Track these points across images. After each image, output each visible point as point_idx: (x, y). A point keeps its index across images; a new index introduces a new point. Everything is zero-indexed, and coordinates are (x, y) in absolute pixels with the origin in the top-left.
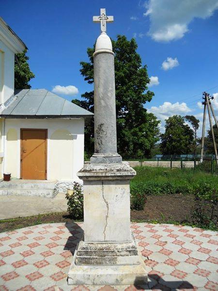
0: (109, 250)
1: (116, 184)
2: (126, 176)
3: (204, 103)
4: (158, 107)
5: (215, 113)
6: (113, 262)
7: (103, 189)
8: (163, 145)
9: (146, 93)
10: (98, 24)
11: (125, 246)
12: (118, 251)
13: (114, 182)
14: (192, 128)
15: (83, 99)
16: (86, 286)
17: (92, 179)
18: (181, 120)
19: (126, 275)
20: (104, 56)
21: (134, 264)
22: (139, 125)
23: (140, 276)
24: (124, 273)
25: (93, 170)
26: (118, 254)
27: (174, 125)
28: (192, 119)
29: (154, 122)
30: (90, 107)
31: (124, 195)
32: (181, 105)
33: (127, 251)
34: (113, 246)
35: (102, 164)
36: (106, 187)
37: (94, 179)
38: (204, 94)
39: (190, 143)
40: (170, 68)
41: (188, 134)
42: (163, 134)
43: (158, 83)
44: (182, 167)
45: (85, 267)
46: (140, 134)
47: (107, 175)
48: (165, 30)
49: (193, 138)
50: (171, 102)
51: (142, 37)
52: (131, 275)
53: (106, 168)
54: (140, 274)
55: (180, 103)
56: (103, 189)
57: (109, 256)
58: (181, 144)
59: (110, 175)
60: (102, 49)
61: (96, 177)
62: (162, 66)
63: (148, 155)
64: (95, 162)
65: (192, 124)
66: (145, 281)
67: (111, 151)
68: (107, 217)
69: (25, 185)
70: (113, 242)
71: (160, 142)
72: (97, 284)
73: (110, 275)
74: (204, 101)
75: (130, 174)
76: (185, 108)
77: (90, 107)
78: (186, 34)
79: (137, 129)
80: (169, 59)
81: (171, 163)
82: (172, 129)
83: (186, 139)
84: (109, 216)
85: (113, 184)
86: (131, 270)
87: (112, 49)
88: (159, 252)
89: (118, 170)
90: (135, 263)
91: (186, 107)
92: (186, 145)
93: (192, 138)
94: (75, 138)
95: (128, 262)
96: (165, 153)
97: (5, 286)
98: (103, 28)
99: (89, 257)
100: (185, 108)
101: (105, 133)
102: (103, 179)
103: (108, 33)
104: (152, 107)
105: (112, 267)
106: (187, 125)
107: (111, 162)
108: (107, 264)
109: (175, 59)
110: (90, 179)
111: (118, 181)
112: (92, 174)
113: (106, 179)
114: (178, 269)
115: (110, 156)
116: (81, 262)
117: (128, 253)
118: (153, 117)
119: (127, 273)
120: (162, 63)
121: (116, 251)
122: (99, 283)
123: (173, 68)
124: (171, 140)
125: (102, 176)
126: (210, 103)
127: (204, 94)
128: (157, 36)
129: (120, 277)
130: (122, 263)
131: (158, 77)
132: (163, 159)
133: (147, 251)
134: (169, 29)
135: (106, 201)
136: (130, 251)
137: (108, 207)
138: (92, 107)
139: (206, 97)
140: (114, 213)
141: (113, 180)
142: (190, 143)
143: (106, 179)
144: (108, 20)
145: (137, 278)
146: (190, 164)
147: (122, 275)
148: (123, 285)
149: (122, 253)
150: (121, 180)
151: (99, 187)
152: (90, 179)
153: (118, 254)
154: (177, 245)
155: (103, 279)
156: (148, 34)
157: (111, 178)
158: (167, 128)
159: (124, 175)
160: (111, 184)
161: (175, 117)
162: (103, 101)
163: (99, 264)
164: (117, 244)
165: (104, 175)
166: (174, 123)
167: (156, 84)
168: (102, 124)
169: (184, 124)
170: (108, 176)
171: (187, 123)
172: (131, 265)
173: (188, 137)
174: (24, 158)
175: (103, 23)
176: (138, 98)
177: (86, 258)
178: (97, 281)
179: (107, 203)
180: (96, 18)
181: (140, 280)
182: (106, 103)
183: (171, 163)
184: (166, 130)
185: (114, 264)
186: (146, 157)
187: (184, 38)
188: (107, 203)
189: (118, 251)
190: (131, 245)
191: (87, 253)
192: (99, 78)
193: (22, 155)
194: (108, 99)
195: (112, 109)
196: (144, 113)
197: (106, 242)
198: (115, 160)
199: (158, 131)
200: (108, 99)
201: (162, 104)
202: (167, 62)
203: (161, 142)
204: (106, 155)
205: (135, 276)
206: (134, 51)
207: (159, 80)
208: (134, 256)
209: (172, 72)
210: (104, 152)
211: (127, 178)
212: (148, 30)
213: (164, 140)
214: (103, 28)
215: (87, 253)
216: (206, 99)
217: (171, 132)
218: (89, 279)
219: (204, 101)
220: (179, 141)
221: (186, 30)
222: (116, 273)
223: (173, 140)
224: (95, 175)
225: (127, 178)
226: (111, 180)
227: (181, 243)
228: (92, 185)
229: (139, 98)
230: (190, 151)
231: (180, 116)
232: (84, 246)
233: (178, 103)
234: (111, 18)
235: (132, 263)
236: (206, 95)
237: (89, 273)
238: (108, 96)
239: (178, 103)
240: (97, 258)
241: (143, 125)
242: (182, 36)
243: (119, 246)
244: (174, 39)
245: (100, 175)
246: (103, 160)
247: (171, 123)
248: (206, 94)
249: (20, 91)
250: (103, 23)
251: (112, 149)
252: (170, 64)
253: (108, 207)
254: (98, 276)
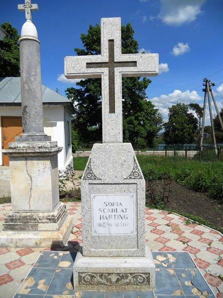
0: (31, 218)
1: (38, 160)
2: (45, 152)
3: (205, 90)
4: (167, 94)
5: (215, 99)
6: (35, 228)
7: (26, 165)
8: (166, 134)
9: (142, 80)
10: (23, 12)
11: (46, 214)
12: (40, 219)
13: (37, 158)
14: (196, 115)
15: (78, 87)
16: (8, 248)
17: (17, 155)
18: (184, 108)
19: (44, 239)
20: (26, 42)
21: (53, 231)
22: (136, 113)
23: (56, 240)
24: (42, 237)
25: (18, 147)
26: (40, 221)
27: (178, 114)
28: (195, 106)
29: (151, 111)
30: (85, 95)
31: (45, 170)
32: (191, 93)
33: (47, 219)
34: (36, 214)
35: (25, 142)
36: (29, 162)
37: (17, 155)
38: (204, 81)
39: (193, 132)
40: (180, 54)
41: (192, 122)
42: (166, 124)
43: (168, 70)
44: (175, 155)
45: (10, 232)
46: (136, 122)
47: (28, 151)
48: (177, 13)
49: (197, 127)
50: (181, 90)
51: (152, 20)
52: (49, 239)
53: (29, 145)
54: (56, 239)
55: (191, 91)
56: (26, 165)
57: (32, 223)
58: (184, 133)
59: (30, 151)
60: (25, 36)
61: (18, 153)
62: (172, 51)
63: (151, 145)
64: (19, 140)
65: (196, 112)
66: (61, 245)
67: (35, 131)
68: (31, 189)
69: (4, 171)
70: (38, 211)
71: (163, 131)
72: (19, 247)
73: (30, 239)
74: (204, 87)
75: (47, 151)
76: (195, 96)
77: (85, 95)
78: (198, 16)
79: (133, 118)
80: (180, 45)
81: (166, 152)
82: (175, 118)
83: (189, 128)
84: (33, 188)
85: (36, 160)
86: (49, 235)
87: (37, 37)
88: (176, 240)
89: (39, 148)
90: (54, 229)
91: (197, 95)
92: (189, 134)
93: (196, 127)
94: (55, 125)
95: (48, 229)
96: (167, 143)
97: (9, 269)
98: (28, 16)
99: (13, 223)
100: (195, 96)
101: (29, 114)
102: (25, 155)
103: (34, 21)
104: (162, 96)
105: (33, 232)
106: (191, 114)
107: (34, 140)
108: (30, 230)
109: (187, 44)
110: (13, 155)
111: (39, 157)
112: (14, 151)
113: (27, 155)
114: (200, 258)
115: (33, 135)
116: (6, 228)
117: (48, 221)
118: (151, 105)
119: (45, 237)
120: (173, 48)
121: (38, 219)
122: (21, 246)
123: (184, 54)
124: (175, 129)
125: (24, 153)
126: (211, 90)
127: (204, 81)
128: (169, 19)
129: (39, 240)
130: (43, 229)
131: (168, 64)
132: (166, 149)
133: (162, 239)
134: (181, 12)
135: (30, 175)
136: (50, 219)
137: (31, 180)
138: (87, 95)
139: (206, 83)
140: (37, 186)
141: (35, 157)
142: (193, 132)
143: (27, 155)
144: (32, 8)
145: (53, 242)
146: (192, 153)
147: (41, 239)
148: (41, 247)
149: (43, 221)
150: (42, 157)
151: (23, 162)
152: (13, 155)
153: (40, 221)
154: (207, 238)
155: (24, 242)
156: (159, 16)
157: (32, 155)
158: (171, 117)
159: (43, 151)
160: (34, 160)
161: (179, 105)
162: (26, 85)
163: (22, 229)
164: (38, 213)
165: (25, 151)
166: (177, 111)
167: (165, 71)
168: (26, 107)
169: (188, 112)
170: (29, 153)
171: (190, 111)
172: (50, 231)
173: (191, 126)
174: (6, 145)
175: (28, 10)
176: (133, 86)
177: (11, 225)
178: (19, 244)
179: (30, 176)
180: (20, 7)
181: (57, 243)
182: (28, 86)
183: (166, 152)
184: (170, 119)
185: (36, 230)
186: (149, 147)
187: (196, 21)
188: (30, 176)
189: (40, 219)
190: (51, 214)
191: (12, 220)
192: (23, 64)
193: (3, 142)
194: (31, 83)
195: (35, 92)
196: (140, 101)
197: (31, 211)
198: (37, 138)
199: (160, 120)
200: (31, 83)
201: (173, 92)
202: (178, 47)
203: (164, 131)
204: (30, 134)
205: (52, 240)
206: (130, 37)
207: (169, 67)
208: (53, 224)
209: (184, 56)
210: (29, 131)
211: (46, 155)
212: (159, 12)
213: (167, 129)
214: (28, 16)
215: (12, 220)
216: (206, 85)
217: (173, 121)
218: (12, 242)
219: (204, 87)
220: (182, 130)
221: (199, 12)
222: (35, 237)
223: (176, 128)
224: (17, 151)
225: (46, 155)
226: (33, 156)
227: (200, 233)
228: (17, 161)
229: (135, 85)
230: (194, 140)
231: (183, 104)
232: (11, 215)
233: (188, 91)
234: (35, 6)
235: (51, 230)
236: (206, 81)
237: (12, 237)
238: (30, 80)
239: (188, 91)
240: (20, 225)
241: (139, 114)
242: (193, 19)
243: (41, 215)
244: (186, 22)
245: (22, 151)
246: (27, 139)
247: (175, 112)
248: (206, 81)
249: (3, 79)
250: (28, 10)
251: (36, 129)
252: (180, 49)
253: (31, 180)
254: (20, 239)
